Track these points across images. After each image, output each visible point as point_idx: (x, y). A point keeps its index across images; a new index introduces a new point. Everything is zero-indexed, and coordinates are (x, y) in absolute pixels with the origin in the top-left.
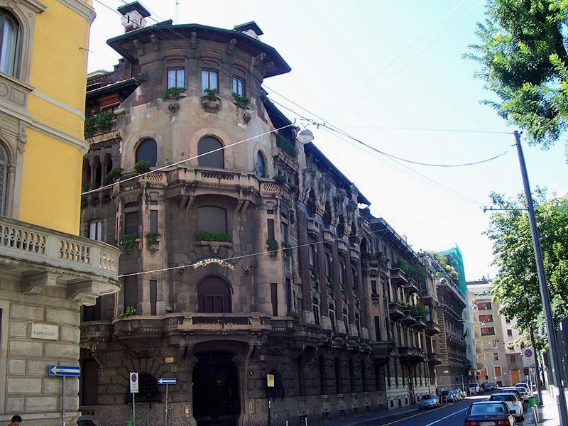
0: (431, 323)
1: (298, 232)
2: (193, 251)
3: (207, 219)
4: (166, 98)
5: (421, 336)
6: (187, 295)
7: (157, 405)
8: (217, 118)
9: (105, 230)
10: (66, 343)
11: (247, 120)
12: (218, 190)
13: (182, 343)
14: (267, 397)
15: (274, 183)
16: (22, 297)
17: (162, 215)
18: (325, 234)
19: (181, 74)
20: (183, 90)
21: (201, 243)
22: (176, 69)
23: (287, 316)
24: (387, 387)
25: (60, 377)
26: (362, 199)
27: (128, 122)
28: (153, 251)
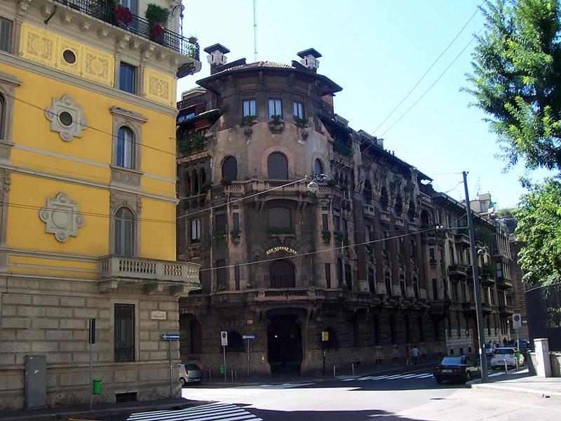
0: (502, 279)
1: (354, 220)
2: (266, 242)
3: (278, 217)
4: (243, 125)
5: (492, 291)
6: (262, 275)
7: (242, 354)
8: (282, 138)
9: (203, 227)
10: (171, 321)
11: (305, 137)
12: (283, 195)
13: (258, 310)
14: (323, 349)
15: (327, 186)
16: (145, 297)
17: (241, 217)
18: (381, 215)
19: (253, 104)
20: (255, 117)
21: (272, 234)
22: (250, 100)
23: (338, 287)
24: (447, 338)
25: (168, 340)
26: (422, 176)
27: (215, 143)
28: (236, 244)
